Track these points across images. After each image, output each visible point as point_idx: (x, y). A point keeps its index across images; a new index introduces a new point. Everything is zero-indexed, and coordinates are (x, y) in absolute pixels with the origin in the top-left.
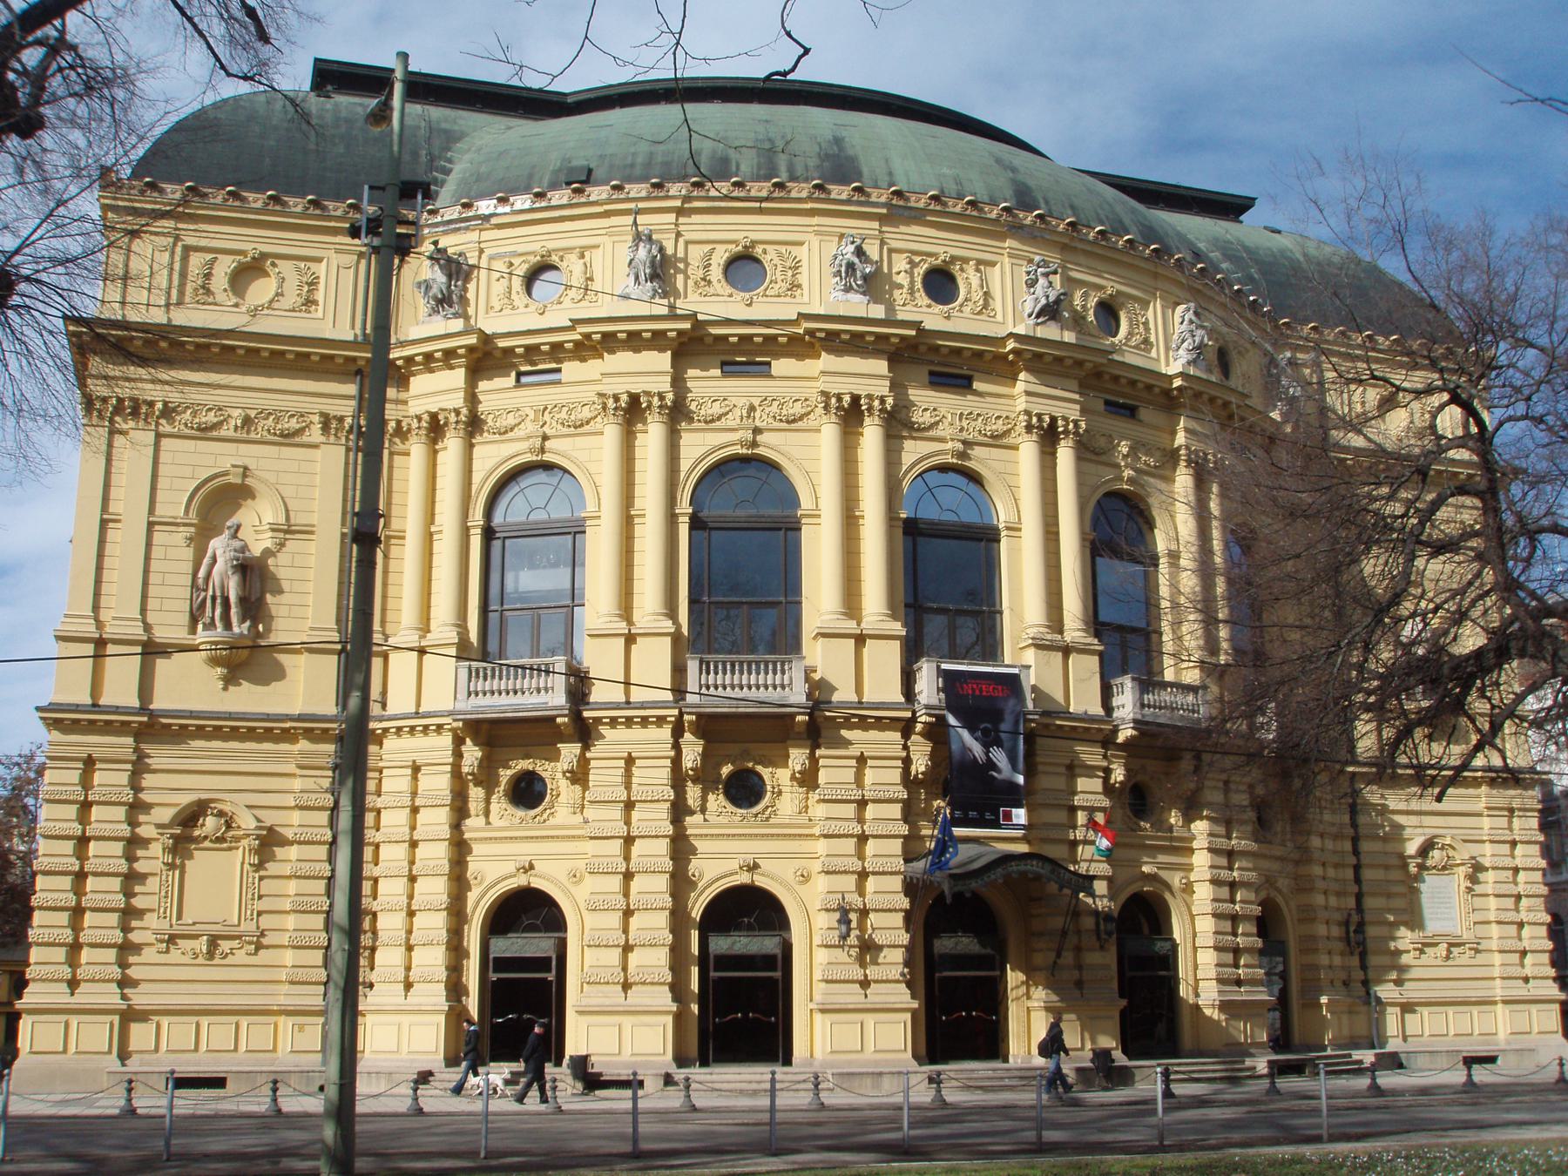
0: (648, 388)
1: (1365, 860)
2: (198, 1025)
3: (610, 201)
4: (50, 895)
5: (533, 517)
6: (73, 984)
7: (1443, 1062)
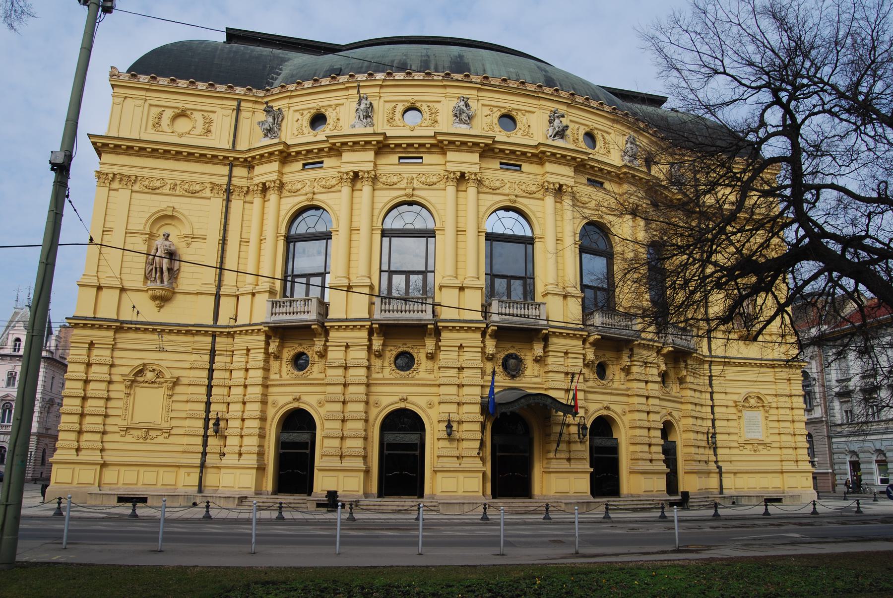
0: (362, 169)
1: (716, 402)
2: (319, 470)
3: (348, 82)
4: (69, 408)
5: (309, 231)
6: (78, 450)
7: (754, 501)
